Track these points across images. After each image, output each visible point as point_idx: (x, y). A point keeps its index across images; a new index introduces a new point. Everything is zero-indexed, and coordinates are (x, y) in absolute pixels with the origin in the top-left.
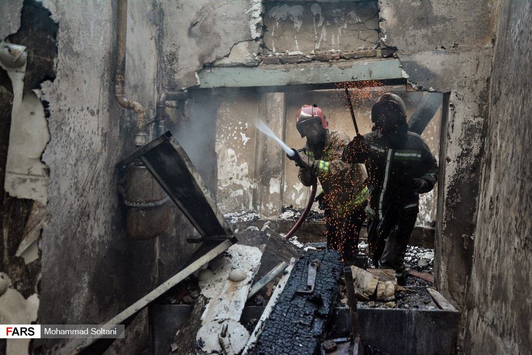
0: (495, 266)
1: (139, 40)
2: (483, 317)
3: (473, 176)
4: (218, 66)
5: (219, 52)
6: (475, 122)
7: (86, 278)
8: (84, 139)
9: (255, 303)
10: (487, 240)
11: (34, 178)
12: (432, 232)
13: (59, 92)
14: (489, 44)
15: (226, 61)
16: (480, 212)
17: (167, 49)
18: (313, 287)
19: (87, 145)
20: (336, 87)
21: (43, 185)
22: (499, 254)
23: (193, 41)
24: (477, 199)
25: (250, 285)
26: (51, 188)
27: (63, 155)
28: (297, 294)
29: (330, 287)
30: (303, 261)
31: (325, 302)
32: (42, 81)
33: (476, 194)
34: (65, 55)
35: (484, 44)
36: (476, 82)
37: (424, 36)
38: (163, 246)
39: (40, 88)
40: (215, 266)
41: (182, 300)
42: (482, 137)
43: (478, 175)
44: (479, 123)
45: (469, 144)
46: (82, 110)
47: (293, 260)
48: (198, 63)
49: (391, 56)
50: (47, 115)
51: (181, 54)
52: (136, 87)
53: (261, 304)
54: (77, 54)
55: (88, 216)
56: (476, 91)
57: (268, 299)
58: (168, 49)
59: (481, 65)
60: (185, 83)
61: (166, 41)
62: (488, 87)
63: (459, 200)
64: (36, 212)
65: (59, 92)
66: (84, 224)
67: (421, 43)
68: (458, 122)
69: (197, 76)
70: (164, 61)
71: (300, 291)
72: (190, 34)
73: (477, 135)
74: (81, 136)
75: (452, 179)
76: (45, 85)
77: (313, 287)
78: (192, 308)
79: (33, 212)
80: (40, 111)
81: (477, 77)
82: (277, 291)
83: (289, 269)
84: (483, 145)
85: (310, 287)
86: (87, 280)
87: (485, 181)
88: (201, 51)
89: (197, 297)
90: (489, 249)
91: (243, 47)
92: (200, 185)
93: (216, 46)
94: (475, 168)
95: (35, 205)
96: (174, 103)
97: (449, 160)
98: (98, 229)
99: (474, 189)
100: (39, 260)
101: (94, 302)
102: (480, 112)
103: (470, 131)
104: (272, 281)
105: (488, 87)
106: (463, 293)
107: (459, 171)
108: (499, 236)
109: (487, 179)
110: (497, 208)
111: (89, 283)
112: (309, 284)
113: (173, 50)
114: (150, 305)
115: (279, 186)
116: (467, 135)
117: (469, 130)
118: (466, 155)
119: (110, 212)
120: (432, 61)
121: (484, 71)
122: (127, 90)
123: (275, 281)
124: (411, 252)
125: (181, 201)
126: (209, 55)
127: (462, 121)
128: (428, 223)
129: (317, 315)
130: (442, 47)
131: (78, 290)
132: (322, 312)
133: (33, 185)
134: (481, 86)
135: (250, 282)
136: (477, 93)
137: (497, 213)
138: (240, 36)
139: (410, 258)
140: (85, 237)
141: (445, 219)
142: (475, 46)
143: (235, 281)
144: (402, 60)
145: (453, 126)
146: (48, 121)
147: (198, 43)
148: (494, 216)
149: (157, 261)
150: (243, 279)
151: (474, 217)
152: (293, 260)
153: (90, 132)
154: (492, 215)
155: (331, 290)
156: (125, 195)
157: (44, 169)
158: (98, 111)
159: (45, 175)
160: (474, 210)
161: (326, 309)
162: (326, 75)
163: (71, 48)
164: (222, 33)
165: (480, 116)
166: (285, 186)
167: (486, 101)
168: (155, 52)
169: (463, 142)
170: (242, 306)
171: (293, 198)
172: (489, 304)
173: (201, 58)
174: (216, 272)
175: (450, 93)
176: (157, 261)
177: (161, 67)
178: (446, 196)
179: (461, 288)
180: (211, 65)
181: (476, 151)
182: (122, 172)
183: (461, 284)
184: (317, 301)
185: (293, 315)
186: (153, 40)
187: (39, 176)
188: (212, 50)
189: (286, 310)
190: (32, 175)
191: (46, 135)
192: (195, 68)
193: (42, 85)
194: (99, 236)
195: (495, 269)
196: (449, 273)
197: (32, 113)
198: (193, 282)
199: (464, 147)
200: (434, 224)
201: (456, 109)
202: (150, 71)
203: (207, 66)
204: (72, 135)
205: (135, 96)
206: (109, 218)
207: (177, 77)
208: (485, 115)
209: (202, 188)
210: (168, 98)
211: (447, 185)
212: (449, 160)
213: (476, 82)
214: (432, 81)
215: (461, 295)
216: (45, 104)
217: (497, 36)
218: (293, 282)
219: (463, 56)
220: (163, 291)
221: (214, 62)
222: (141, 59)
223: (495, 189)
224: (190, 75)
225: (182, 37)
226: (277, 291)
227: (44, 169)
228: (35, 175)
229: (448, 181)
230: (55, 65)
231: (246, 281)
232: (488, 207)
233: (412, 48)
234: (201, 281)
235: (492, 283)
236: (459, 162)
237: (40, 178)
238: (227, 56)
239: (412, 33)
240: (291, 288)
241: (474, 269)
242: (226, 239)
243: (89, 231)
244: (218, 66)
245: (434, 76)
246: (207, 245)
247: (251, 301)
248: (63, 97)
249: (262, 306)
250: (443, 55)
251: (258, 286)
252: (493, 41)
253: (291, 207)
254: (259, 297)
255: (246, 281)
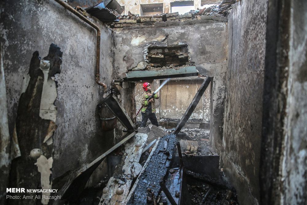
0: (231, 137)
1: (106, 62)
2: (227, 155)
3: (222, 106)
4: (133, 70)
5: (133, 66)
6: (222, 87)
7: (87, 145)
8: (84, 96)
9: (145, 155)
10: (228, 128)
11: (51, 111)
12: (209, 124)
13: (73, 80)
14: (225, 61)
15: (136, 69)
16: (225, 118)
17: (116, 65)
18: (166, 149)
19: (85, 98)
20: (181, 80)
21: (55, 114)
22: (233, 133)
23: (125, 62)
24: (224, 114)
25: (143, 149)
26: (71, 114)
27: (75, 102)
28: (160, 152)
29: (172, 148)
30: (163, 139)
31: (170, 154)
32: (55, 74)
33: (224, 112)
34: (76, 67)
35: (224, 60)
36: (222, 73)
37: (204, 58)
38: (117, 132)
39: (54, 76)
40: (131, 141)
41: (118, 154)
42: (225, 92)
43: (224, 105)
44: (223, 87)
45: (221, 95)
46: (83, 86)
47: (159, 138)
48: (126, 69)
49: (193, 65)
50: (57, 86)
51: (121, 66)
52: (104, 78)
53: (147, 155)
54: (81, 67)
55: (87, 123)
56: (222, 76)
57: (150, 153)
58: (116, 65)
59: (223, 68)
60: (122, 76)
61: (116, 63)
62: (226, 75)
63: (218, 114)
64: (51, 125)
65: (73, 80)
66: (85, 127)
67: (204, 60)
68: (217, 87)
69: (126, 74)
70: (115, 70)
71: (161, 150)
72: (124, 60)
73: (223, 92)
74: (82, 96)
75: (215, 107)
76: (56, 76)
77: (166, 149)
78: (122, 157)
79: (50, 125)
80: (54, 85)
81: (222, 72)
82: (154, 149)
83: (157, 142)
84: (225, 95)
85: (165, 149)
86: (87, 146)
87: (226, 107)
88: (127, 66)
89: (124, 153)
90: (229, 131)
91: (141, 63)
92: (124, 112)
93: (132, 64)
94: (223, 103)
95: (51, 122)
96: (118, 83)
97: (214, 100)
98: (91, 128)
99: (222, 111)
100: (53, 144)
101: (90, 154)
102: (224, 84)
103: (221, 90)
104: (152, 146)
105: (226, 75)
106: (220, 146)
107: (218, 104)
108: (233, 127)
109: (227, 107)
110: (231, 117)
111: (88, 147)
112: (165, 147)
113: (118, 65)
114: (107, 156)
115: (159, 111)
116: (220, 92)
117: (220, 90)
118: (220, 99)
119: (96, 122)
120: (207, 66)
121: (224, 70)
122: (101, 79)
123: (152, 147)
124: (202, 131)
125: (119, 117)
126: (130, 67)
127: (218, 87)
128: (207, 121)
129: (167, 159)
130: (210, 62)
131: (84, 150)
132: (169, 158)
133: (50, 114)
134: (224, 74)
135: (143, 147)
136: (223, 77)
137: (231, 118)
138: (141, 60)
139: (202, 133)
140: (86, 131)
141: (214, 121)
142: (221, 61)
143: (137, 146)
144: (196, 66)
145: (215, 88)
146: (57, 89)
147: (126, 63)
148: (230, 120)
149: (115, 138)
150: (140, 146)
151: (223, 120)
152: (159, 138)
153: (87, 94)
154: (229, 120)
155: (173, 149)
156: (101, 116)
157: (55, 108)
158: (90, 87)
159: (55, 110)
160: (223, 118)
161: (170, 157)
162: (170, 72)
163: (79, 65)
164: (134, 59)
165: (224, 85)
166: (161, 111)
167: (226, 80)
168: (112, 66)
169: (218, 94)
170: (140, 156)
171: (164, 114)
172: (230, 151)
173: (128, 68)
174: (131, 143)
175: (213, 77)
176: (115, 138)
177: (114, 71)
178: (213, 113)
179: (219, 145)
180: (131, 70)
181: (223, 97)
182: (99, 108)
183: (219, 143)
184: (167, 154)
185: (158, 159)
186: (111, 62)
187: (53, 110)
188: (131, 65)
189: (156, 158)
190: (51, 110)
191: (56, 94)
192: (126, 71)
193: (55, 75)
194: (91, 130)
195: (231, 139)
196: (215, 140)
197: (51, 86)
198: (123, 147)
199: (219, 96)
200: (209, 121)
201: (216, 82)
202: (110, 72)
203: (129, 70)
204: (79, 95)
205: (105, 81)
206: (95, 124)
207: (119, 75)
208: (226, 85)
209: (125, 113)
210: (115, 81)
211: (214, 109)
212: (214, 100)
213: (222, 73)
214: (207, 73)
215: (219, 147)
216: (56, 82)
217: (228, 58)
218: (159, 147)
219: (217, 65)
220: (111, 151)
221: (132, 69)
222: (106, 69)
223: (230, 110)
224: (124, 74)
225: (121, 61)
226: (154, 149)
227: (55, 108)
228: (52, 110)
229: (238, 149)
230: (61, 68)
231: (141, 147)
232: (228, 116)
233: (200, 62)
234: (126, 147)
235: (230, 143)
236: (217, 101)
237: (53, 111)
238: (136, 67)
239: (200, 57)
240: (158, 149)
241: (223, 138)
242: (134, 131)
243: (87, 129)
244: (133, 70)
245: (208, 71)
246: (129, 133)
247: (143, 154)
248: (75, 82)
249: (147, 157)
250: (210, 64)
251: (146, 149)
252: (227, 59)
253: (163, 117)
254: (147, 153)
255: (141, 147)
